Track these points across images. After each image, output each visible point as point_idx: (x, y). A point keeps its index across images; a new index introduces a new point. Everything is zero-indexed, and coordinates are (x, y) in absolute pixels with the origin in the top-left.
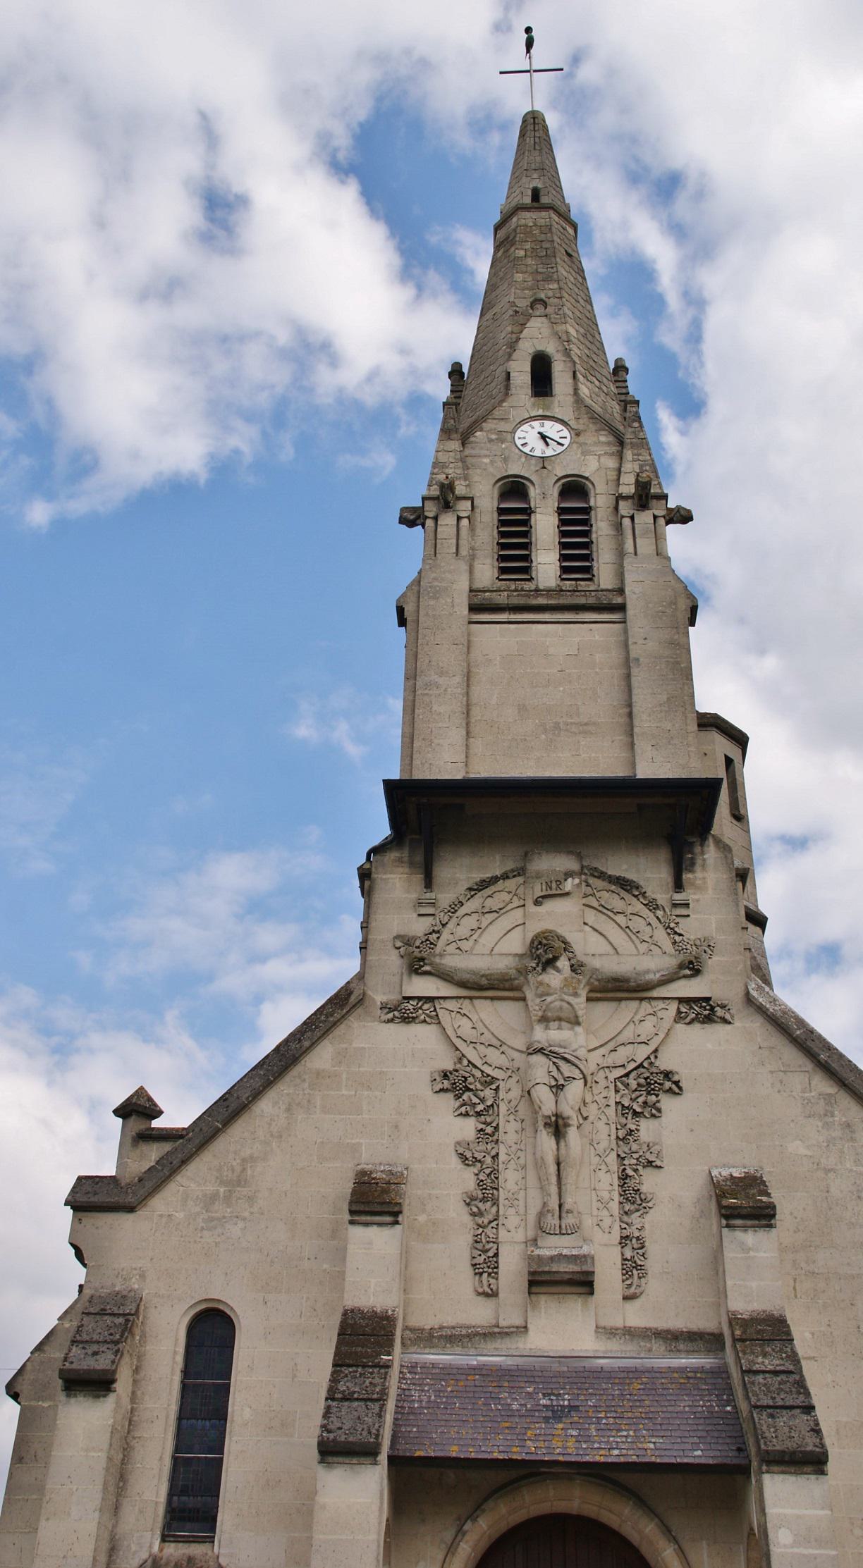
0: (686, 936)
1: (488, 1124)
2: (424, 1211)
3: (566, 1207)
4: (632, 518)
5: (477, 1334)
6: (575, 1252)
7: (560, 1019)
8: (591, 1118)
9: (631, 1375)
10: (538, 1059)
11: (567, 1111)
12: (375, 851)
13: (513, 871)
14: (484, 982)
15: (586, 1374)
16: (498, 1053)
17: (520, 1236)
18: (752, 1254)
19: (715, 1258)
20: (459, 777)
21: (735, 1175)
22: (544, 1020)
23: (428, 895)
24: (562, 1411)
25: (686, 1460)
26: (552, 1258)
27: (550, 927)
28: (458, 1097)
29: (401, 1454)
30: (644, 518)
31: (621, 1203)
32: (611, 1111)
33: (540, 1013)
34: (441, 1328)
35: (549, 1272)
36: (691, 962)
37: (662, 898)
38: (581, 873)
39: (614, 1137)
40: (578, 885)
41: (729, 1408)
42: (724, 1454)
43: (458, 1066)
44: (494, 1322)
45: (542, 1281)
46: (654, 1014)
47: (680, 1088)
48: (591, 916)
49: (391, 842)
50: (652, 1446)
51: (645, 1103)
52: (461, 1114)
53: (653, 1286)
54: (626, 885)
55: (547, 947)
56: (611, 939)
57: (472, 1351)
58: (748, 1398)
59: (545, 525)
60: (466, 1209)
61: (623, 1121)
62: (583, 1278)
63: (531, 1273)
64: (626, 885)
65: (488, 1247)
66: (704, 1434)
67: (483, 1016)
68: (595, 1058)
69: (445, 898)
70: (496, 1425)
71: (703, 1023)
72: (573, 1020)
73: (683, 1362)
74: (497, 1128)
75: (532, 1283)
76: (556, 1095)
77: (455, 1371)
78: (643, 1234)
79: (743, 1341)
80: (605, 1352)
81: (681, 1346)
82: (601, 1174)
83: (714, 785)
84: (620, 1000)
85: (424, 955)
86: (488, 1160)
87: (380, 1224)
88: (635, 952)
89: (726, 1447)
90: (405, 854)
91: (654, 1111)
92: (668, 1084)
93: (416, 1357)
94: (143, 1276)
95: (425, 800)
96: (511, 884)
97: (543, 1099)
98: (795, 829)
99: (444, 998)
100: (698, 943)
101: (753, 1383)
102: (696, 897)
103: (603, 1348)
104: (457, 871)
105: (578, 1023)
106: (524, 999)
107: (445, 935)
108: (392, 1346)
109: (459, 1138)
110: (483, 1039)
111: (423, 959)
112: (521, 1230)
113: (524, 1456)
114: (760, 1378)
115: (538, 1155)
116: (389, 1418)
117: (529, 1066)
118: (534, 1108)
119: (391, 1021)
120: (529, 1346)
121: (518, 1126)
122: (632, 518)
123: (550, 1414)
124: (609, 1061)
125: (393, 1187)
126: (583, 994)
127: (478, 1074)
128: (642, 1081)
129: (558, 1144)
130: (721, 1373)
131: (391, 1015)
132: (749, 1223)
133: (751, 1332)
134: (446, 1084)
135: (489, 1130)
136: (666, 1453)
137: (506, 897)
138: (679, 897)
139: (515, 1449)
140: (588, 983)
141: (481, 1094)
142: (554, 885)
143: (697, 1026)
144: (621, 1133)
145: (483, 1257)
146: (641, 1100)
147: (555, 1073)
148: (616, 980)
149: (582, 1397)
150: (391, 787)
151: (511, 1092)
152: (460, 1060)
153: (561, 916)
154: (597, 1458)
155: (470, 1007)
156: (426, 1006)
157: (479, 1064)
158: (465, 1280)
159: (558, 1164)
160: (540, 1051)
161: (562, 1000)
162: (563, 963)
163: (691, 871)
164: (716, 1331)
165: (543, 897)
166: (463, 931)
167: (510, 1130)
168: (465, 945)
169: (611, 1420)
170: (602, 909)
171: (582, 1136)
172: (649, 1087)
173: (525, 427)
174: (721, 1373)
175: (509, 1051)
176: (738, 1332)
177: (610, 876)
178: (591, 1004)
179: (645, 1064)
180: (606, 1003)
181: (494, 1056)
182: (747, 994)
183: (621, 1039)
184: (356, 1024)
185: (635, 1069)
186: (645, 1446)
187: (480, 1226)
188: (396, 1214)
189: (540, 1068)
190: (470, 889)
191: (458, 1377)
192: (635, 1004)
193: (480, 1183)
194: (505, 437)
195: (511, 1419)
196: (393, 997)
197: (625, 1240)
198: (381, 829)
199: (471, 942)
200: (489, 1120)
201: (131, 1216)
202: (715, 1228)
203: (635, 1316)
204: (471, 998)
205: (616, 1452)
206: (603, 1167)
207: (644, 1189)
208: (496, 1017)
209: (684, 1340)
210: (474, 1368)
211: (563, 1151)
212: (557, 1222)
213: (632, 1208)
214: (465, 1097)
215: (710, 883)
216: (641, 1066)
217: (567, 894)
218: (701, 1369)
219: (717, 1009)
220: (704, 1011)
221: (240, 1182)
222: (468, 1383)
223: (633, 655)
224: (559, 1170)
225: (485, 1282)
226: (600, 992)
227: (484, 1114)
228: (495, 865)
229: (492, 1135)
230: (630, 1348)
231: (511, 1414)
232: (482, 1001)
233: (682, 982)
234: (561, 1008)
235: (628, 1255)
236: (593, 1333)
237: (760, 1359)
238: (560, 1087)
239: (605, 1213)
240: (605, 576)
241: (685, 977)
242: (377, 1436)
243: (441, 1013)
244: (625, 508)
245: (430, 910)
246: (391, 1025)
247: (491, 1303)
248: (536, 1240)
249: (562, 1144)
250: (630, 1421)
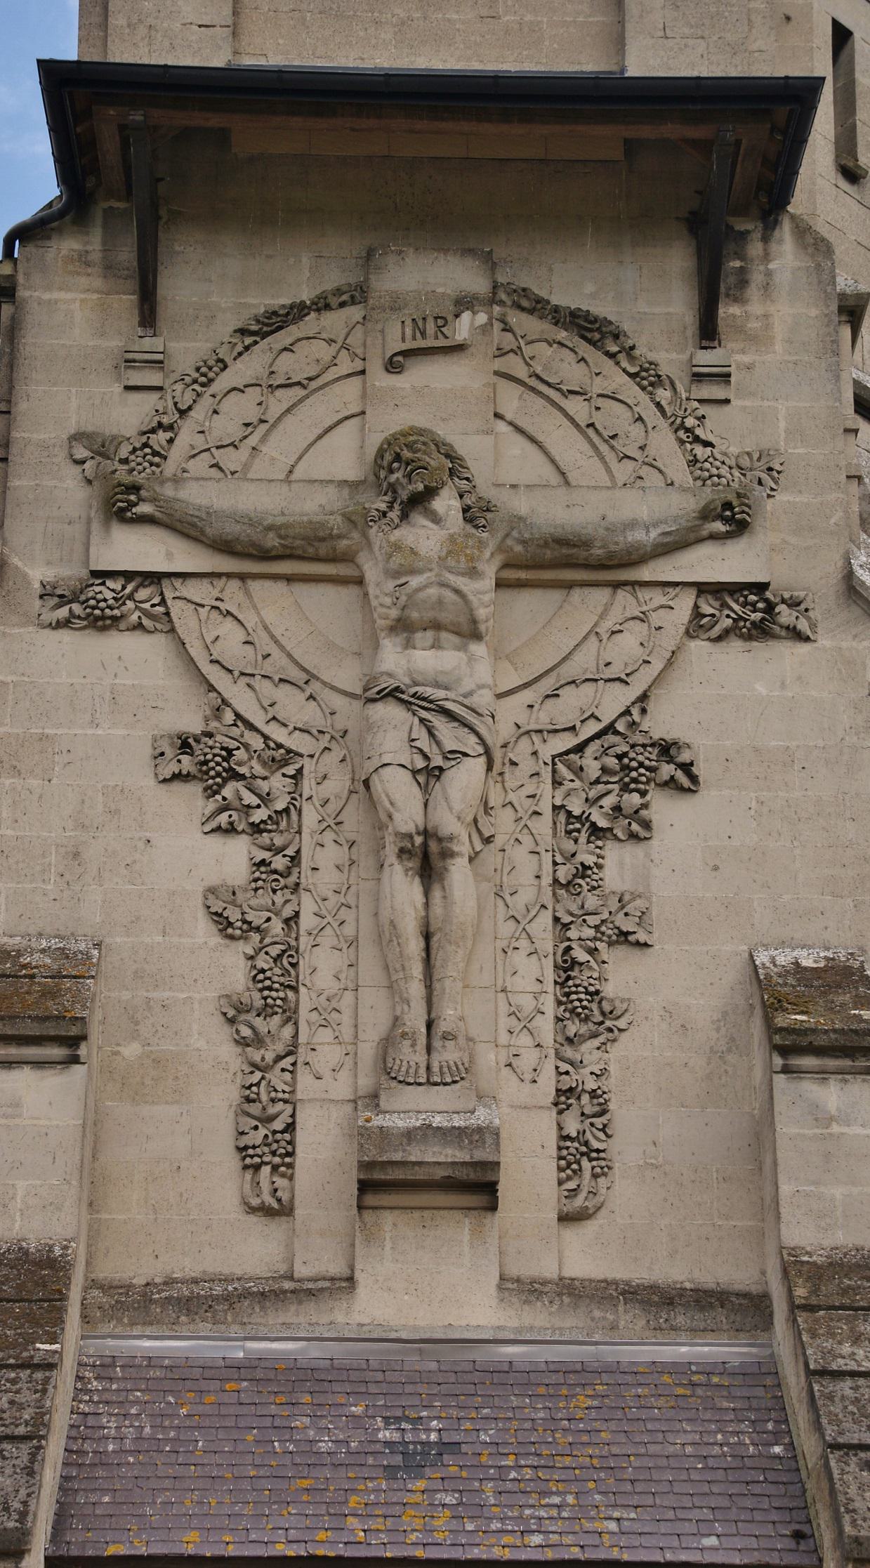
0: (721, 446)
1: (279, 851)
2: (135, 1036)
3: (442, 1027)
5: (247, 1294)
6: (458, 1122)
7: (437, 626)
8: (499, 841)
9: (572, 1379)
10: (389, 712)
11: (449, 823)
12: (22, 234)
13: (338, 292)
14: (272, 541)
15: (476, 1377)
16: (301, 697)
17: (341, 1088)
18: (835, 1129)
19: (757, 1135)
20: (218, 61)
21: (807, 962)
22: (403, 627)
23: (148, 343)
24: (425, 1454)
25: (683, 1557)
26: (409, 1135)
27: (421, 422)
28: (211, 792)
29: (75, 1552)
31: (559, 1020)
32: (543, 826)
33: (394, 613)
34: (169, 1282)
35: (403, 1164)
36: (728, 505)
38: (493, 300)
39: (547, 880)
40: (486, 329)
41: (777, 1449)
42: (764, 1543)
43: (214, 724)
44: (283, 1268)
45: (381, 1184)
46: (642, 618)
47: (694, 779)
48: (511, 400)
49: (61, 214)
50: (613, 1526)
51: (617, 808)
52: (218, 829)
53: (625, 1193)
54: (590, 329)
55: (413, 468)
56: (554, 452)
57: (235, 1330)
58: (818, 1427)
60: (227, 1030)
61: (569, 846)
62: (472, 1176)
63: (365, 1166)
64: (590, 329)
65: (272, 1110)
66: (725, 1502)
67: (270, 616)
68: (512, 712)
69: (186, 349)
70: (282, 1485)
71: (749, 638)
72: (465, 628)
73: (682, 1351)
74: (295, 859)
75: (365, 1187)
76: (425, 789)
77: (197, 1373)
78: (605, 1084)
79: (810, 1308)
80: (519, 1330)
81: (680, 1320)
83: (796, 97)
84: (569, 586)
85: (139, 478)
86: (277, 927)
87: (38, 1064)
88: (605, 480)
89: (770, 1530)
90: (94, 242)
91: (635, 827)
92: (667, 770)
93: (112, 1345)
95: (137, 117)
96: (335, 322)
97: (397, 797)
99: (184, 576)
100: (745, 462)
101: (830, 1397)
102: (746, 359)
103: (514, 1323)
104: (214, 285)
105: (476, 636)
106: (360, 581)
107: (187, 437)
108: (60, 1321)
109: (213, 880)
110: (267, 668)
111: (136, 488)
112: (344, 1075)
113: (341, 1550)
114: (845, 1387)
115: (385, 914)
116: (50, 1476)
117: (369, 726)
118: (378, 818)
120: (357, 1318)
121: (341, 855)
123: (398, 1460)
124: (542, 718)
125: (68, 983)
126: (490, 571)
127: (257, 743)
128: (612, 762)
129: (427, 893)
130: (764, 1375)
131: (63, 612)
132: (831, 1063)
133: (829, 1291)
134: (187, 764)
135: (279, 863)
136: (645, 1541)
137: (322, 351)
138: (706, 358)
139: (322, 1536)
140: (500, 549)
141: (264, 786)
142: (431, 327)
143: (736, 644)
144: (564, 873)
145: (262, 1131)
146: (608, 802)
147: (424, 742)
148: (561, 542)
149: (468, 1425)
150: (58, 80)
151: (327, 782)
153: (439, 399)
154: (497, 1553)
155: (240, 596)
156: (143, 594)
157: (258, 720)
158: (223, 1183)
159: (427, 937)
160: (393, 694)
161: (443, 585)
162: (447, 503)
163: (739, 300)
164: (755, 1289)
165: (406, 354)
166: (226, 427)
167: (323, 863)
168: (231, 460)
169: (528, 1473)
171: (479, 877)
172: (628, 775)
174: (764, 1375)
175: (326, 695)
176: (800, 1292)
177: (556, 309)
178: (507, 595)
179: (620, 727)
180: (538, 593)
181: (292, 704)
182: (849, 575)
183: (569, 671)
185: (598, 736)
186: (598, 1526)
187: (255, 1066)
188: (74, 1042)
189: (393, 730)
190: (243, 332)
191: (203, 1385)
193: (258, 977)
195: (315, 1472)
196: (68, 572)
197: (565, 1096)
198: (39, 185)
199: (244, 453)
200: (279, 841)
202: (758, 1074)
203: (583, 1254)
204: (243, 577)
205: (537, 1539)
206: (523, 943)
207: (609, 990)
208: (297, 617)
209: (686, 1306)
210: (238, 1367)
211: (437, 909)
212: (421, 1058)
213: (584, 1029)
214: (228, 791)
216: (610, 729)
217: (460, 348)
218: (722, 1368)
219: (782, 608)
220: (753, 613)
222: (226, 1398)
224: (428, 949)
225: (266, 1187)
226: (527, 567)
227: (269, 828)
228: (299, 273)
229: (286, 874)
230: (572, 1322)
231: (315, 1460)
232: (268, 584)
234: (440, 602)
235: (572, 1128)
236: (493, 1290)
237: (846, 1348)
238: (434, 773)
239: (525, 1039)
241: (713, 537)
242: (23, 1515)
243: (176, 608)
245: (153, 378)
246: (65, 635)
247: (276, 1229)
248: (375, 1096)
249: (437, 894)
250: (569, 1475)
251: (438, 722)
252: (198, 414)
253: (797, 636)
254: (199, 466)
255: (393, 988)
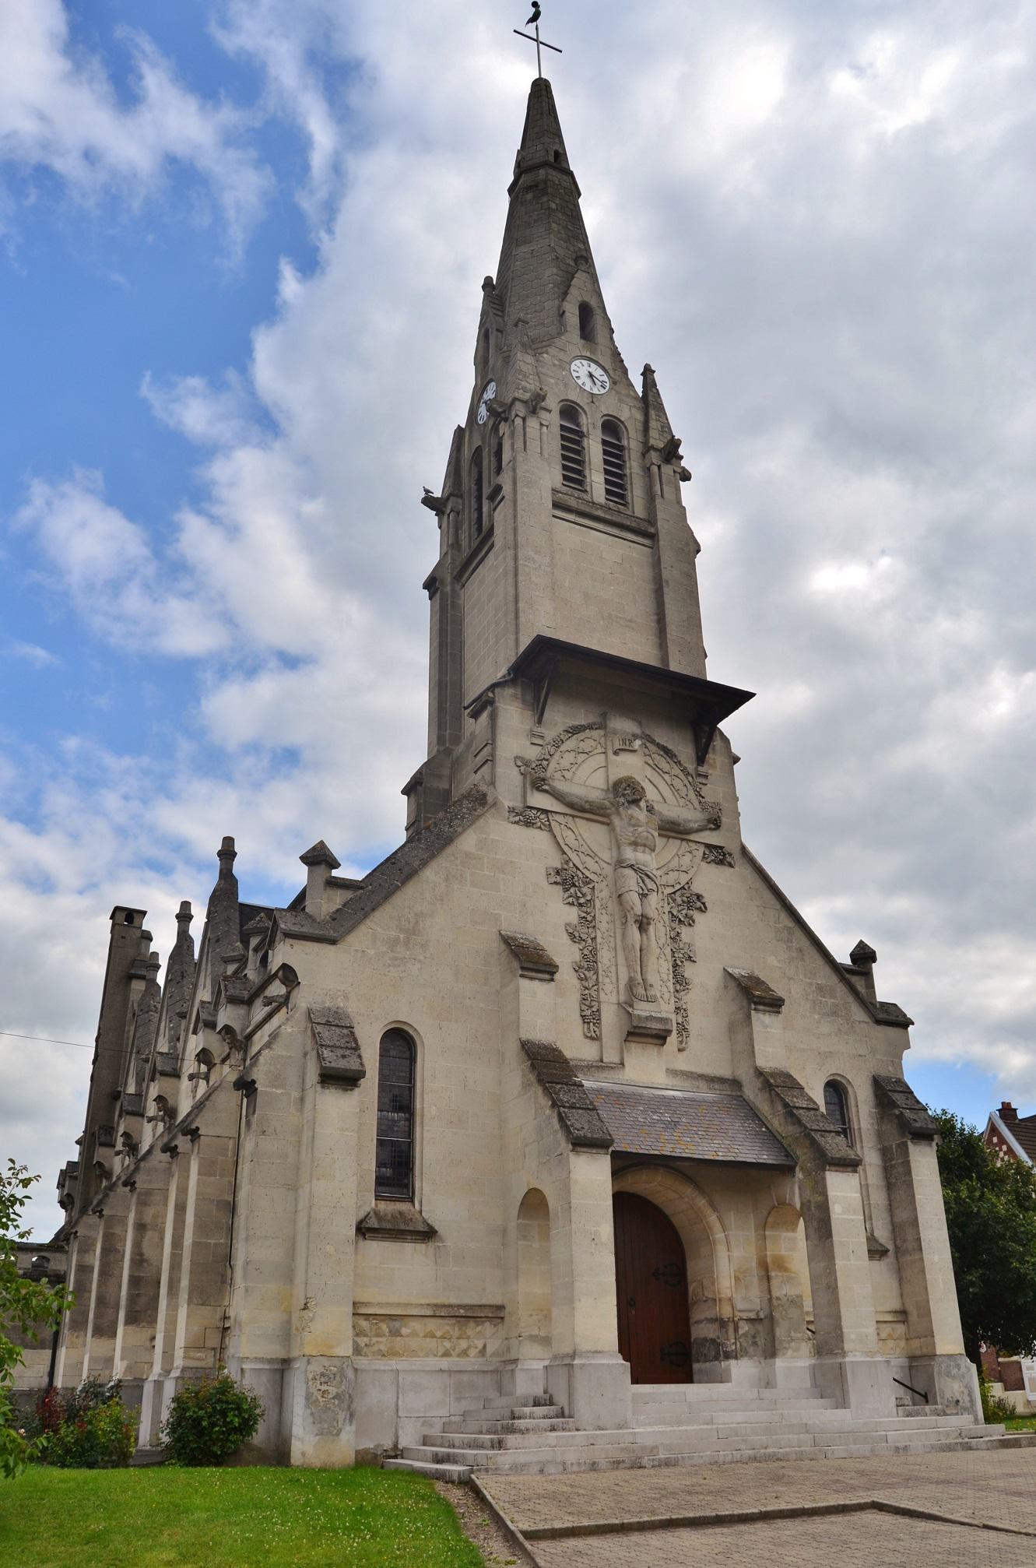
4: (524, 419)
14: (587, 806)
22: (635, 844)
26: (647, 1018)
28: (566, 890)
30: (667, 470)
32: (666, 917)
37: (691, 767)
53: (693, 1043)
54: (668, 753)
59: (594, 449)
60: (575, 975)
69: (550, 732)
75: (630, 1034)
82: (662, 961)
84: (669, 837)
87: (541, 980)
92: (699, 904)
94: (346, 997)
96: (596, 734)
98: (293, 647)
104: (560, 716)
107: (553, 765)
112: (614, 995)
119: (516, 823)
122: (524, 419)
134: (559, 879)
137: (594, 744)
144: (673, 934)
152: (567, 863)
162: (643, 804)
167: (603, 920)
170: (656, 768)
173: (585, 362)
181: (590, 863)
184: (491, 821)
188: (552, 974)
192: (678, 842)
194: (564, 366)
196: (518, 804)
201: (332, 948)
203: (683, 1063)
208: (591, 835)
214: (572, 890)
215: (718, 764)
221: (415, 931)
223: (664, 576)
233: (707, 833)
240: (639, 508)
243: (553, 824)
244: (654, 457)
245: (540, 742)
247: (595, 1045)
251: (647, 881)
252: (557, 756)
253: (731, 865)
254: (558, 775)
255: (629, 967)
